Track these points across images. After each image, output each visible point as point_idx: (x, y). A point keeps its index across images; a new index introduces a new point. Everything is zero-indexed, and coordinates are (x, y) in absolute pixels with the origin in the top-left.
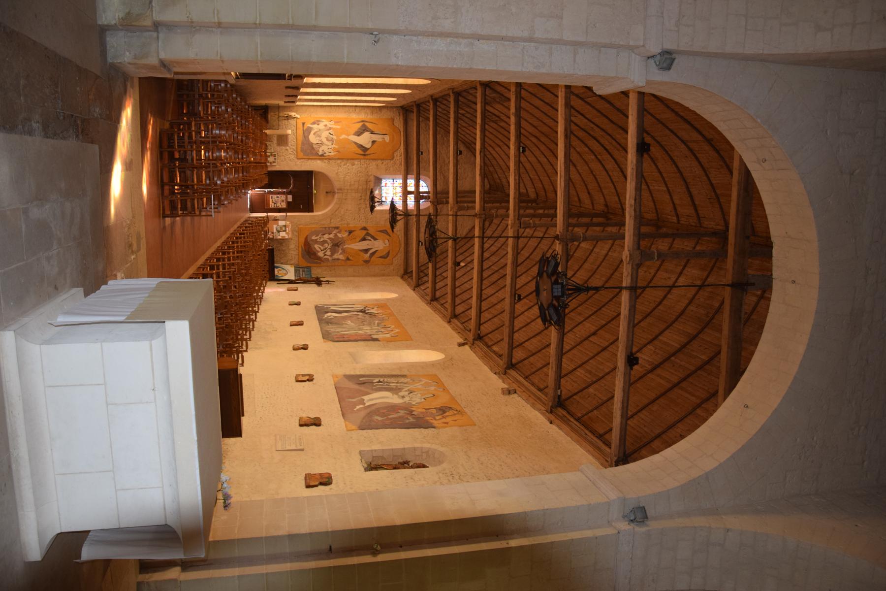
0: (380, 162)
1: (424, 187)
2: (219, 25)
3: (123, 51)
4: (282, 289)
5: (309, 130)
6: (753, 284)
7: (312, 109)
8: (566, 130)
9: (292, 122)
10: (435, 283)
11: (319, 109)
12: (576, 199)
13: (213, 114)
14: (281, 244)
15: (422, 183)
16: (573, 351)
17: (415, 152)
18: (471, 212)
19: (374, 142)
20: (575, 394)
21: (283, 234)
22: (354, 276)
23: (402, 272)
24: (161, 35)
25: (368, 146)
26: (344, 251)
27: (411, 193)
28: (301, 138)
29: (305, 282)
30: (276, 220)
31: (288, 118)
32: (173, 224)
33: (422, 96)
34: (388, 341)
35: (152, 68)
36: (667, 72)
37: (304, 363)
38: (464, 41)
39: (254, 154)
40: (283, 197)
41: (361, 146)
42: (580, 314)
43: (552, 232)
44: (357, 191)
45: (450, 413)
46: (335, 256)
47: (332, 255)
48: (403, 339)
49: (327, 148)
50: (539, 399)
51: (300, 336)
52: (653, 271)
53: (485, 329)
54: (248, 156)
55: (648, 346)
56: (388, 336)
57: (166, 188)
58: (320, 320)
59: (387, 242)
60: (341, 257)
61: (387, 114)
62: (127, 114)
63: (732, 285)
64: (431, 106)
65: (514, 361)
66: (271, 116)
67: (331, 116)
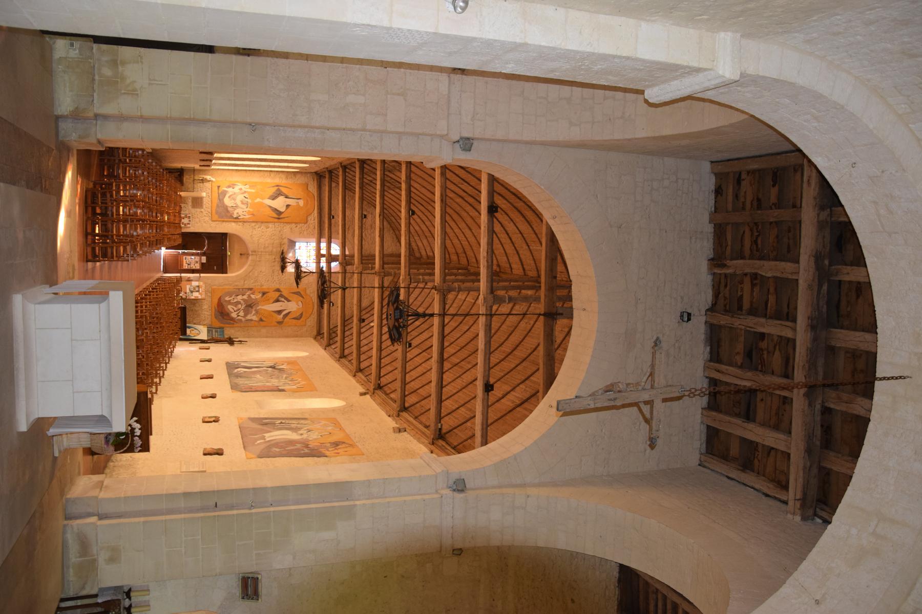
0: (293, 225)
1: (336, 250)
2: (141, 117)
3: (72, 134)
4: (194, 348)
5: (224, 193)
6: (562, 314)
7: (227, 173)
8: (441, 195)
9: (207, 185)
10: (343, 343)
11: (234, 173)
12: (474, 260)
13: (130, 177)
14: (194, 304)
15: (333, 245)
16: (459, 394)
17: (327, 216)
18: (373, 271)
19: (288, 206)
20: (455, 428)
21: (196, 295)
22: (267, 337)
23: (315, 333)
24: (99, 122)
25: (282, 209)
26: (257, 312)
27: (323, 256)
28: (216, 201)
29: (217, 341)
30: (189, 280)
31: (203, 181)
32: (94, 268)
33: (332, 163)
34: (294, 391)
35: (92, 144)
36: (468, 153)
37: (210, 408)
38: (317, 131)
39: (168, 214)
40: (197, 258)
41: (275, 210)
42: (469, 363)
43: (430, 285)
44: (271, 253)
45: (344, 445)
46: (249, 317)
47: (246, 315)
48: (309, 389)
49: (241, 211)
50: (423, 433)
51: (209, 387)
52: (532, 322)
53: (384, 381)
54: (162, 215)
55: (521, 386)
56: (295, 387)
57: (89, 237)
58: (230, 374)
59: (300, 303)
60: (255, 318)
61: (301, 180)
62: (69, 176)
63: (544, 315)
64: (341, 173)
65: (407, 405)
66: (186, 178)
67: (246, 180)
